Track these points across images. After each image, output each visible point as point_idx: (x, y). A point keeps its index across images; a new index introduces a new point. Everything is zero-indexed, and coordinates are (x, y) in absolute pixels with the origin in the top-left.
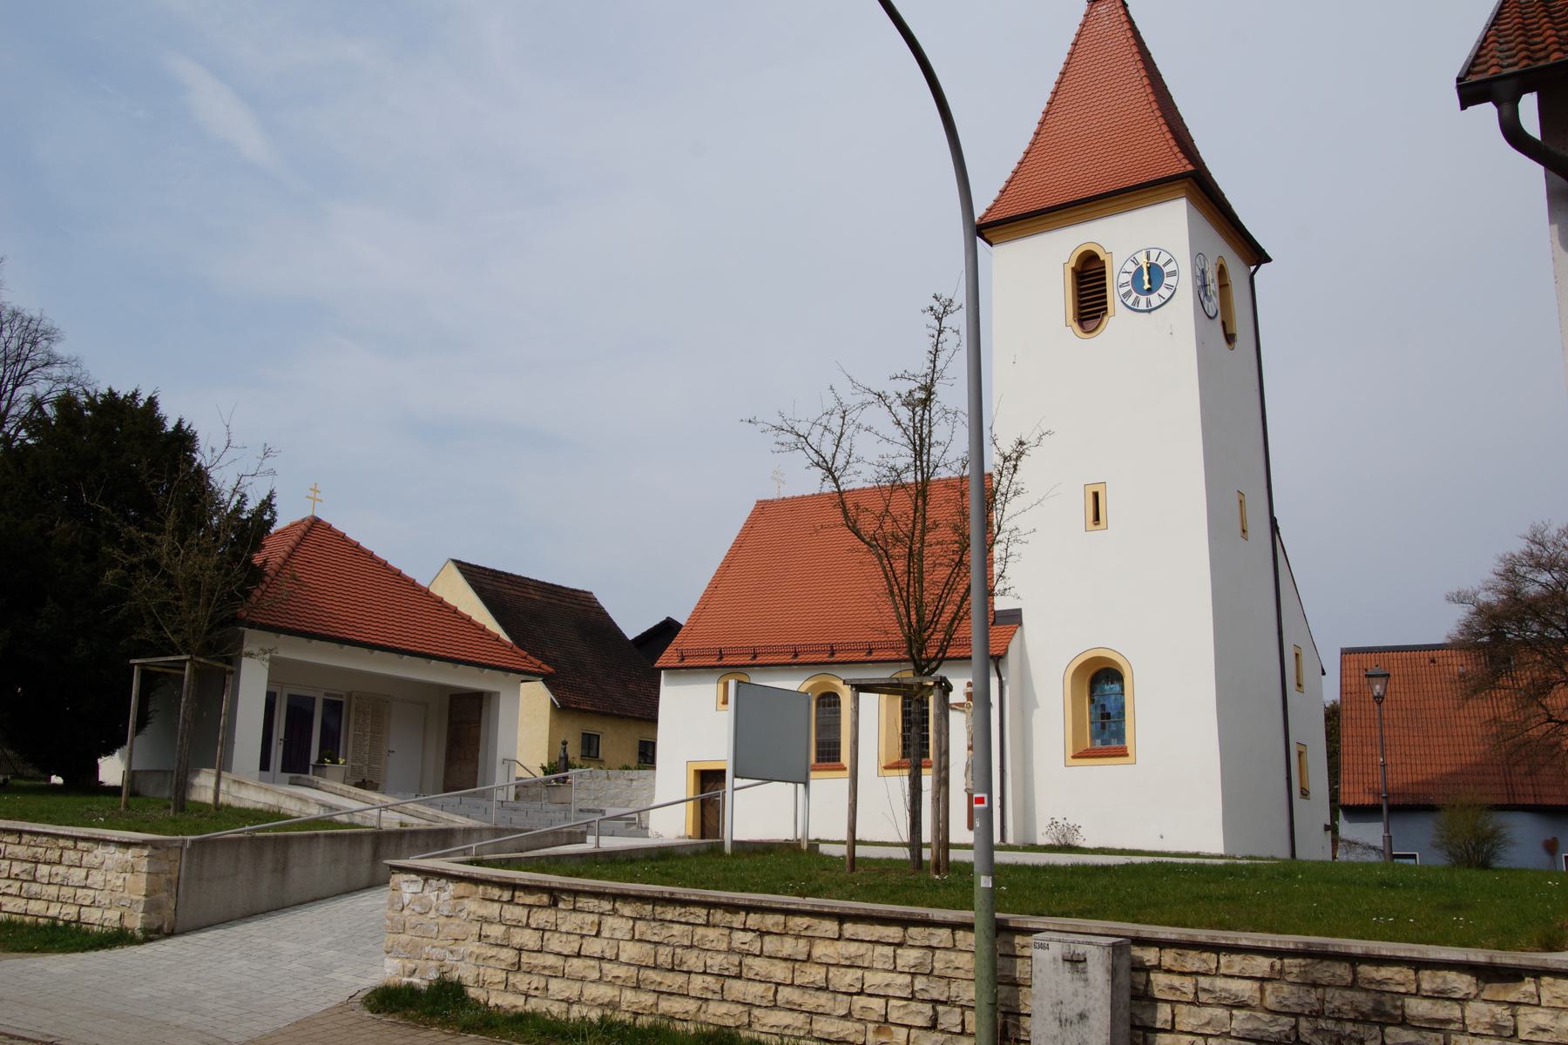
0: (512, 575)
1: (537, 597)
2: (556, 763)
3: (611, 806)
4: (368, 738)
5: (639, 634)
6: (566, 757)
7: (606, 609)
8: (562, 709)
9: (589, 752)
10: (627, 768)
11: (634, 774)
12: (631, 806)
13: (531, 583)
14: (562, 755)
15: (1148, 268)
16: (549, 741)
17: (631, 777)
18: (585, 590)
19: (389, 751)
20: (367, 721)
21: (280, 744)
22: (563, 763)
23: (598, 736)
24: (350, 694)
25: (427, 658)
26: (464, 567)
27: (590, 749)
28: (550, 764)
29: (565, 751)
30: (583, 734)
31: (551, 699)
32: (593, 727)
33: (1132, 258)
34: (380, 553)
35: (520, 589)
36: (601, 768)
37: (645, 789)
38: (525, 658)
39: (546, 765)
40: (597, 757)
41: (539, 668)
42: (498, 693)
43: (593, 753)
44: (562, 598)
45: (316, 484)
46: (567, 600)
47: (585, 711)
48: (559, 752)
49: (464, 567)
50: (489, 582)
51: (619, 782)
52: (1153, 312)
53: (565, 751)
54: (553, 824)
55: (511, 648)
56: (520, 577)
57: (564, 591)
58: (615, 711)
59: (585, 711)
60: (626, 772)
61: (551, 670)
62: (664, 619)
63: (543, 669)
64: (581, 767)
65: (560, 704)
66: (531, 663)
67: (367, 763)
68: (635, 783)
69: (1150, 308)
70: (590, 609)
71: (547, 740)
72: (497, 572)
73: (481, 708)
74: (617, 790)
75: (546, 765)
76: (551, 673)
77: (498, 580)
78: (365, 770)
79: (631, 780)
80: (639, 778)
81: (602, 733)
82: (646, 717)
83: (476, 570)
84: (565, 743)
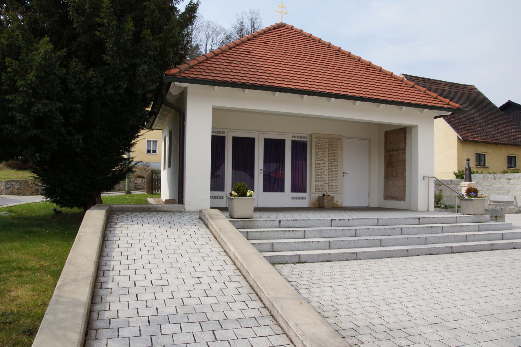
0: (433, 80)
1: (447, 89)
2: (463, 171)
3: (497, 194)
4: (327, 165)
5: (501, 105)
6: (470, 169)
7: (482, 93)
8: (464, 141)
9: (480, 164)
10: (506, 172)
11: (511, 176)
12: (509, 194)
13: (443, 83)
14: (467, 167)
16: (458, 159)
17: (509, 178)
18: (471, 85)
19: (344, 173)
20: (325, 153)
21: (261, 173)
22: (468, 172)
23: (485, 155)
24: (311, 136)
25: (353, 100)
26: (408, 77)
27: (481, 160)
28: (459, 172)
29: (468, 165)
30: (476, 154)
31: (458, 136)
32: (482, 150)
34: (326, 39)
35: (438, 86)
36: (489, 173)
37: (518, 185)
38: (436, 98)
39: (457, 172)
40: (485, 165)
41: (448, 104)
42: (416, 126)
43: (482, 164)
44: (459, 89)
45: (282, 3)
46: (462, 89)
47: (477, 142)
48: (465, 166)
49: (408, 77)
50: (421, 83)
51: (501, 180)
53: (468, 165)
54: (465, 237)
55: (425, 92)
56: (437, 80)
57: (460, 86)
58: (493, 141)
59: (477, 142)
60: (506, 174)
61: (457, 105)
62: (507, 101)
63: (451, 105)
64: (477, 173)
65: (463, 138)
66: (441, 101)
67: (327, 182)
68: (511, 181)
70: (474, 93)
71: (457, 158)
72: (425, 79)
73: (405, 139)
74: (500, 185)
75: (457, 172)
76: (458, 108)
77: (427, 82)
78: (326, 187)
79: (509, 179)
80: (514, 178)
81: (486, 153)
82: (511, 143)
83: (414, 78)
84: (468, 160)
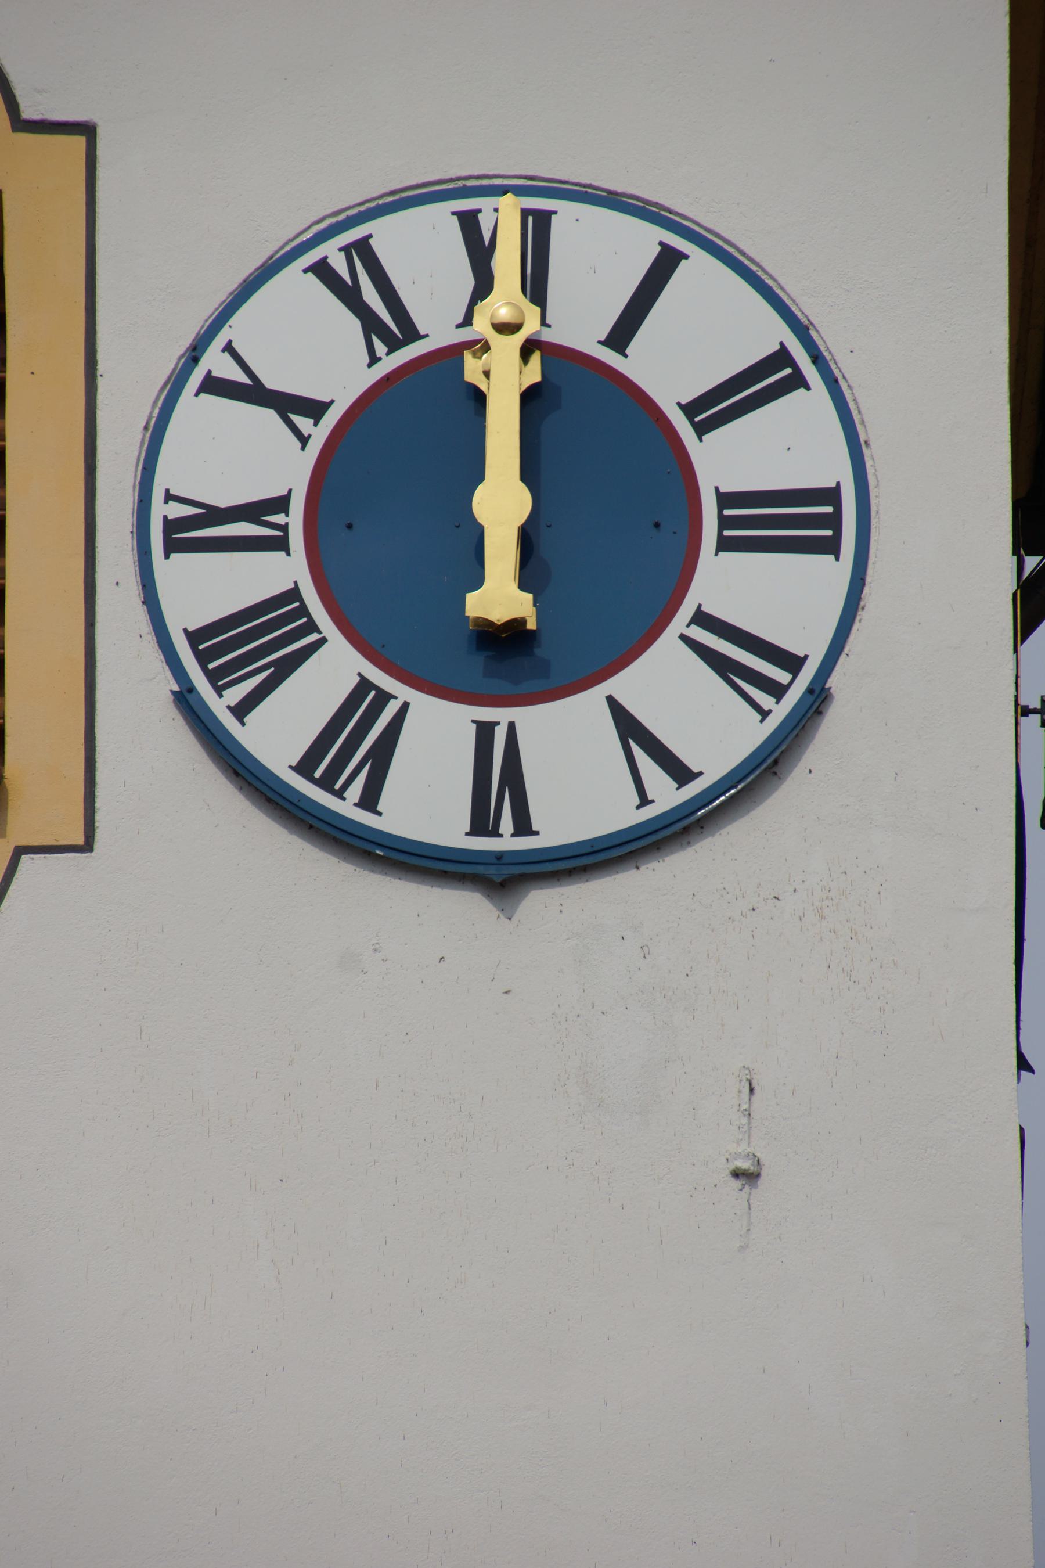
15: (529, 397)
33: (332, 251)
52: (1019, 674)
69: (507, 842)
